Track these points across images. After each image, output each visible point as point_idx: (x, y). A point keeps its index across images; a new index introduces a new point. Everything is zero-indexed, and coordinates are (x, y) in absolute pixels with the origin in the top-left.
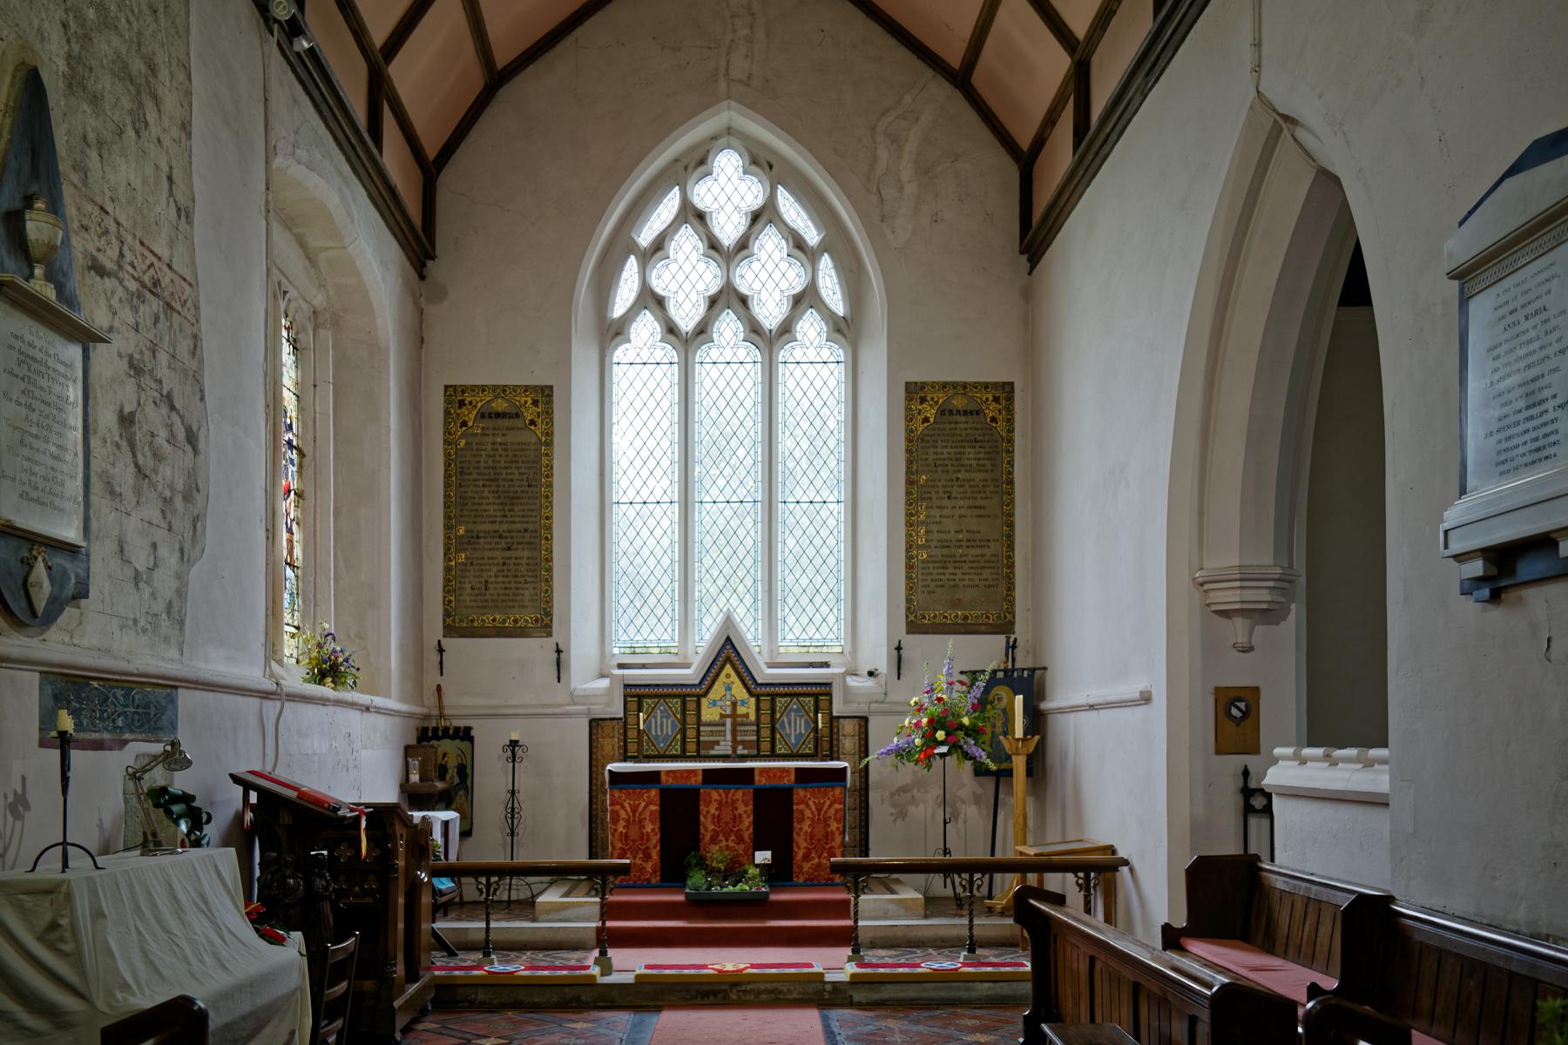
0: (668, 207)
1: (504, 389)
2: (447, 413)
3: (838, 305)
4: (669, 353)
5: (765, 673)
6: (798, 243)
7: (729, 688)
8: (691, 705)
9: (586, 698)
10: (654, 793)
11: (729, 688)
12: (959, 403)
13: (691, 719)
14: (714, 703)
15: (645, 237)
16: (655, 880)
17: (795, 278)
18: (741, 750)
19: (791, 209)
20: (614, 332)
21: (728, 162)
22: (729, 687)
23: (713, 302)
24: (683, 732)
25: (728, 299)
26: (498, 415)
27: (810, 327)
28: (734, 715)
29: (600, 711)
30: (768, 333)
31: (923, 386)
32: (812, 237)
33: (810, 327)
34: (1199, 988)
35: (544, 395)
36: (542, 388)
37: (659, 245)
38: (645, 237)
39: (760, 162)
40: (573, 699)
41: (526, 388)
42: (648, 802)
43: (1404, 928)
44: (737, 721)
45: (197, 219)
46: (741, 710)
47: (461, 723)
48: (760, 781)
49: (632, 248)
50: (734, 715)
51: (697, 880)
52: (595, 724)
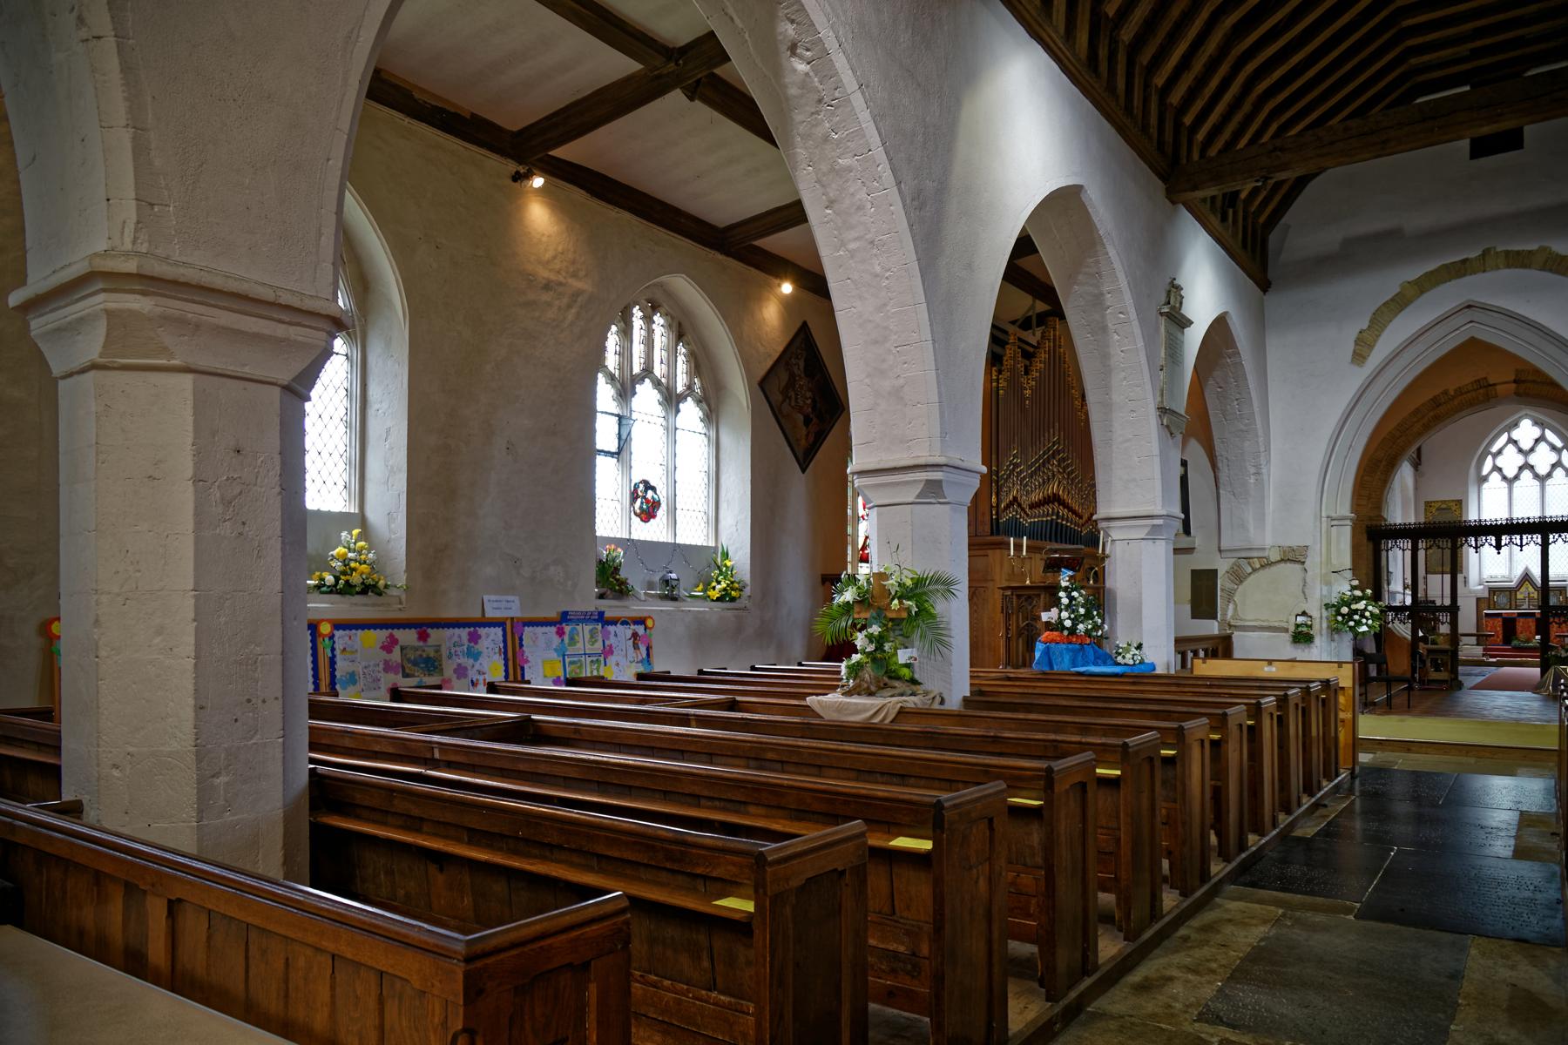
1: (1445, 501)
2: (1425, 509)
4: (1505, 484)
6: (1554, 448)
8: (1513, 593)
9: (1475, 591)
10: (1500, 619)
11: (1527, 588)
14: (1521, 593)
15: (1494, 449)
16: (1501, 643)
18: (1531, 607)
19: (1550, 435)
20: (1485, 479)
21: (1526, 424)
25: (1527, 466)
26: (1444, 509)
29: (1480, 595)
32: (1559, 444)
34: (429, 772)
35: (1459, 502)
36: (1458, 501)
37: (1500, 452)
38: (1494, 449)
39: (1536, 423)
40: (1470, 592)
41: (1453, 501)
42: (1498, 623)
43: (540, 727)
44: (1531, 599)
45: (10, 118)
46: (1532, 595)
47: (1432, 599)
48: (1504, 616)
49: (1490, 453)
51: (1515, 643)
52: (1478, 600)
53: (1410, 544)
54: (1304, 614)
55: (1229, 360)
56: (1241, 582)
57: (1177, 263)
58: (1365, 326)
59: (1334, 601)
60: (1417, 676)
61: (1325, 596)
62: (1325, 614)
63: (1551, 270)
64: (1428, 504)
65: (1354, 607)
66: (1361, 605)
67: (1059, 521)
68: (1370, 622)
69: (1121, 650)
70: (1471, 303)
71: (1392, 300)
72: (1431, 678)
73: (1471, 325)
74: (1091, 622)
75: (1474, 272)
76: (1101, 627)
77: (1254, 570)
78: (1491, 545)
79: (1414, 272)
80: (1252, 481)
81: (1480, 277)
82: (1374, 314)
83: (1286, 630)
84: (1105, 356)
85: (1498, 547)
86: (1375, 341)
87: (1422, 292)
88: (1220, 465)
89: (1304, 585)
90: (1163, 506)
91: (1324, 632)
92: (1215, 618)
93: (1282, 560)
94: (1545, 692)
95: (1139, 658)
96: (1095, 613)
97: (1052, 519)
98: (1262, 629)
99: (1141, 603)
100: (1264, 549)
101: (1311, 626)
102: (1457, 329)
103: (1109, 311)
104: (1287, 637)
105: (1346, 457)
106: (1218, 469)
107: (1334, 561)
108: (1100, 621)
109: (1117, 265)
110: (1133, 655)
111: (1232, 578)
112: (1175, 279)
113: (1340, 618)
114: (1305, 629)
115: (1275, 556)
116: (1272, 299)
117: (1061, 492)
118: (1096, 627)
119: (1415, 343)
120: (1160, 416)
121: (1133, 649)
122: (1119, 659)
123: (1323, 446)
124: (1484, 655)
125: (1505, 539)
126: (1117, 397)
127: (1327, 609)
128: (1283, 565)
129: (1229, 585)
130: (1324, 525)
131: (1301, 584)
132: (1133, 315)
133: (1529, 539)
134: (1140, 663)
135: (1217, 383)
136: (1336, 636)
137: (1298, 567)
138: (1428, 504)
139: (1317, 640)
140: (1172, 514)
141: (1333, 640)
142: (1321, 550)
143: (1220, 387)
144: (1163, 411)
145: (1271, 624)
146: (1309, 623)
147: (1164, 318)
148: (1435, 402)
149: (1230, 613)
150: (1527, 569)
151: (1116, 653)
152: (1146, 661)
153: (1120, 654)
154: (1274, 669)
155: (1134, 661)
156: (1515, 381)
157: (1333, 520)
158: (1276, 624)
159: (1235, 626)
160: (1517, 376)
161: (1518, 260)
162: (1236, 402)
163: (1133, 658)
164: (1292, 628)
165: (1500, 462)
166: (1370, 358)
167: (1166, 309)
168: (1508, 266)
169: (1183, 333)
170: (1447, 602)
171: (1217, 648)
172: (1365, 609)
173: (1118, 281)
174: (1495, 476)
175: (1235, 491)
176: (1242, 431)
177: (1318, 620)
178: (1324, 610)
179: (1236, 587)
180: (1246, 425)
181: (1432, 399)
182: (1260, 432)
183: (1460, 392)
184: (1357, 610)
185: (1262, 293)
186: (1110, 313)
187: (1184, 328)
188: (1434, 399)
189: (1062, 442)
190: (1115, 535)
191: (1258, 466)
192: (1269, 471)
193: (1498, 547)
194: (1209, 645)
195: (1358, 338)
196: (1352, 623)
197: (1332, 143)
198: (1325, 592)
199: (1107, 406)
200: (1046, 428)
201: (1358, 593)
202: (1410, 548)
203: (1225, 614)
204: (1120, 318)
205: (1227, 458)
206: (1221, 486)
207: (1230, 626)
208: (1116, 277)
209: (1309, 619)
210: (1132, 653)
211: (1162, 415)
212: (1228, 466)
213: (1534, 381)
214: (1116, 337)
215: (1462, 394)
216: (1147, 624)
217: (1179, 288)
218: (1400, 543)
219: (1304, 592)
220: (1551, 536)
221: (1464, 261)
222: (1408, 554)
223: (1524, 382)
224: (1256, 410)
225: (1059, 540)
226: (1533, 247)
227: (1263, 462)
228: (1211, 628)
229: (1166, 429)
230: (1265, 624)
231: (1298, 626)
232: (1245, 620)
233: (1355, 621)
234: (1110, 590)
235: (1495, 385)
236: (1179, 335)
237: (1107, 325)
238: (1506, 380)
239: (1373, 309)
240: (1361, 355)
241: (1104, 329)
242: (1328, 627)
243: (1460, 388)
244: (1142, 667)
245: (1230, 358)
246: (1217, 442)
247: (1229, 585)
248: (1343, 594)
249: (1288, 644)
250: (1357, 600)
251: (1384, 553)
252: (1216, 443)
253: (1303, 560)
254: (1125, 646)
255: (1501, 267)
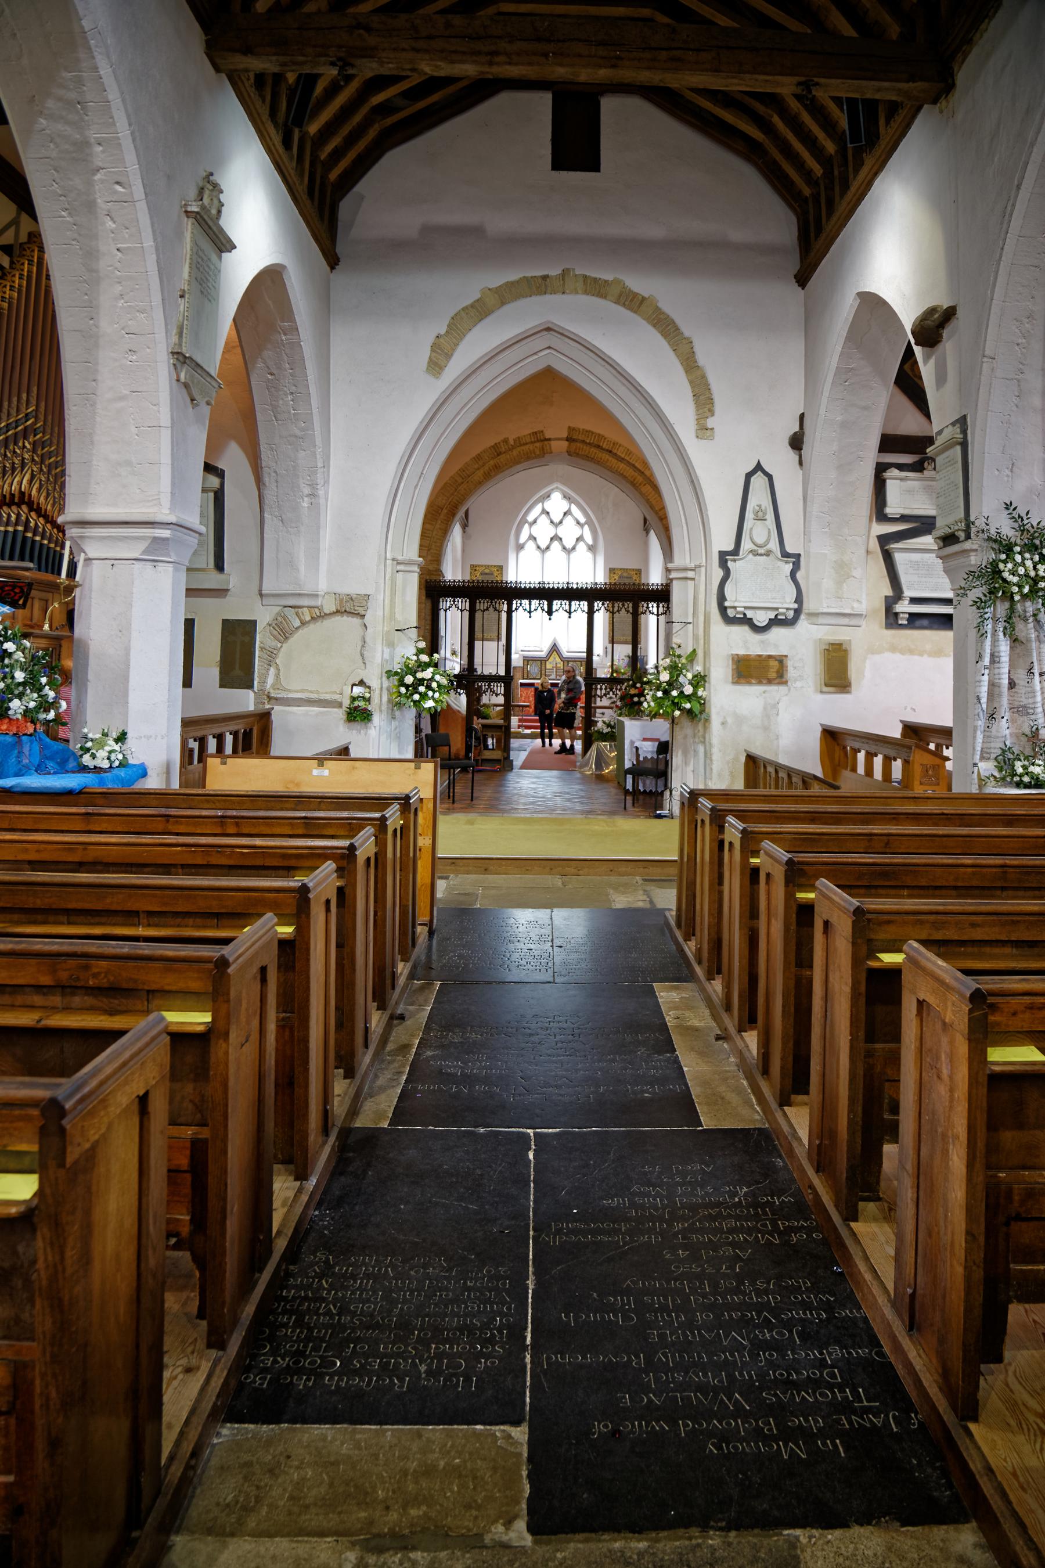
0: (538, 509)
3: (590, 542)
5: (566, 654)
7: (555, 659)
8: (543, 663)
10: (533, 689)
12: (625, 574)
13: (543, 668)
17: (577, 532)
19: (574, 509)
20: (520, 547)
21: (556, 496)
22: (555, 659)
23: (552, 539)
24: (541, 671)
25: (556, 538)
27: (582, 547)
28: (556, 667)
30: (812, 883)
31: (614, 569)
32: (582, 520)
33: (582, 547)
37: (535, 522)
38: (530, 518)
39: (566, 497)
42: (531, 692)
49: (527, 522)
50: (556, 667)
53: (468, 604)
54: (361, 683)
55: (284, 338)
56: (287, 638)
57: (221, 159)
58: (443, 332)
59: (397, 668)
60: (472, 755)
61: (387, 661)
62: (386, 683)
63: (624, 305)
64: (474, 568)
65: (419, 675)
66: (427, 674)
67: (29, 535)
68: (437, 695)
69: (89, 744)
70: (550, 326)
71: (472, 306)
72: (484, 757)
73: (548, 351)
74: (35, 695)
75: (554, 292)
76: (54, 704)
77: (303, 623)
78: (543, 610)
79: (497, 278)
80: (305, 505)
81: (558, 298)
82: (453, 318)
83: (340, 705)
84: (91, 255)
85: (550, 612)
86: (454, 350)
87: (503, 303)
88: (266, 479)
89: (363, 646)
90: (172, 509)
91: (384, 708)
92: (250, 686)
93: (338, 612)
94: (589, 770)
95: (120, 757)
96: (44, 680)
97: (16, 531)
98: (310, 702)
99: (128, 666)
100: (317, 596)
101: (369, 700)
102: (535, 353)
103: (98, 177)
104: (340, 714)
105: (416, 487)
106: (264, 484)
107: (399, 617)
108: (52, 694)
109: (113, 94)
110: (110, 752)
111: (275, 633)
112: (212, 174)
113: (403, 690)
114: (362, 704)
115: (329, 606)
116: (340, 278)
117: (34, 492)
118: (45, 705)
119: (493, 361)
120: (174, 365)
121: (111, 742)
122: (86, 759)
123: (392, 467)
124: (519, 727)
125: (556, 604)
126: (107, 326)
127: (388, 678)
128: (338, 618)
129: (272, 643)
130: (389, 570)
131: (360, 644)
132: (138, 191)
133: (621, 606)
134: (121, 765)
135: (268, 367)
136: (397, 713)
137: (356, 621)
138: (474, 568)
139: (376, 719)
140: (183, 523)
141: (394, 718)
142: (384, 601)
143: (271, 374)
144: (180, 358)
145: (323, 697)
146: (367, 695)
147: (191, 220)
148: (496, 451)
149: (270, 680)
150: (555, 639)
151: (81, 748)
152: (131, 761)
153: (88, 750)
154: (326, 772)
155: (111, 762)
156: (567, 439)
157: (398, 563)
158: (328, 697)
159: (276, 699)
160: (569, 434)
161: (596, 288)
162: (290, 397)
163: (109, 758)
164: (347, 702)
165: (535, 531)
166: (447, 369)
167: (195, 208)
168: (586, 292)
169: (220, 258)
170: (502, 672)
171: (251, 730)
172: (432, 679)
173: (114, 124)
174: (531, 544)
175: (284, 516)
176: (296, 436)
177: (378, 692)
178: (384, 679)
179: (279, 645)
180: (302, 430)
181: (493, 446)
182: (318, 441)
183: (519, 442)
184: (423, 680)
185: (328, 269)
186: (102, 181)
187: (222, 251)
188: (495, 447)
189: (49, 430)
190: (92, 550)
191: (313, 486)
192: (327, 493)
193: (550, 612)
194: (240, 727)
195: (434, 344)
196: (416, 697)
197: (430, 37)
198: (386, 656)
199: (91, 338)
200: (15, 391)
201: (424, 658)
202: (468, 608)
203: (263, 682)
204: (116, 192)
205: (275, 472)
206: (266, 508)
207: (270, 698)
208: (112, 117)
209: (367, 690)
210: (108, 748)
211: (178, 365)
212: (277, 482)
213: (583, 442)
214: (110, 224)
215: (521, 445)
216: (135, 700)
217: (217, 189)
218: (459, 601)
219: (362, 655)
220: (596, 604)
221: (545, 278)
222: (466, 614)
223: (574, 440)
224: (315, 411)
225: (56, 571)
226: (608, 276)
227: (321, 481)
228: (245, 701)
229: (184, 391)
230: (314, 696)
231: (354, 699)
232: (289, 691)
233: (420, 694)
234: (80, 641)
235: (549, 440)
236: (214, 257)
237: (94, 202)
238: (560, 436)
239: (452, 314)
240: (436, 364)
241: (90, 206)
242: (390, 701)
243: (519, 438)
244: (122, 773)
245: (285, 334)
246: (263, 448)
247: (272, 643)
248: (408, 658)
249: (342, 722)
250: (422, 666)
251: (442, 613)
252: (262, 448)
253: (363, 613)
254: (98, 736)
255: (580, 292)
